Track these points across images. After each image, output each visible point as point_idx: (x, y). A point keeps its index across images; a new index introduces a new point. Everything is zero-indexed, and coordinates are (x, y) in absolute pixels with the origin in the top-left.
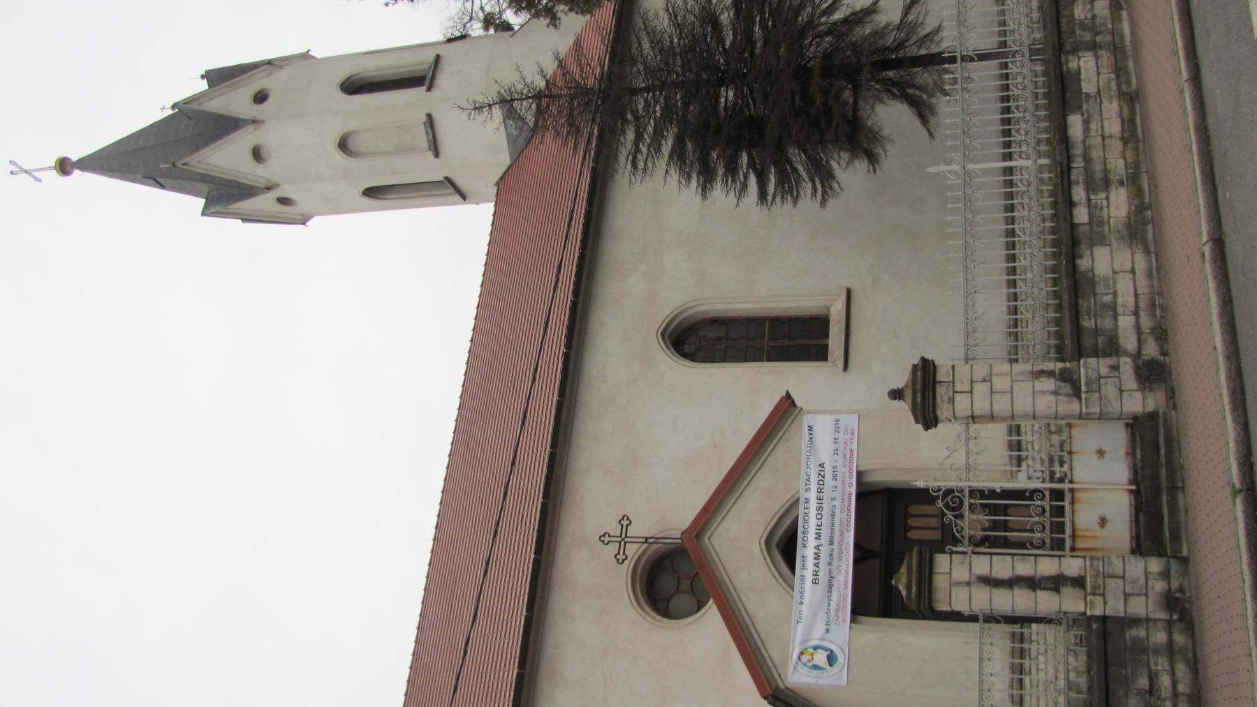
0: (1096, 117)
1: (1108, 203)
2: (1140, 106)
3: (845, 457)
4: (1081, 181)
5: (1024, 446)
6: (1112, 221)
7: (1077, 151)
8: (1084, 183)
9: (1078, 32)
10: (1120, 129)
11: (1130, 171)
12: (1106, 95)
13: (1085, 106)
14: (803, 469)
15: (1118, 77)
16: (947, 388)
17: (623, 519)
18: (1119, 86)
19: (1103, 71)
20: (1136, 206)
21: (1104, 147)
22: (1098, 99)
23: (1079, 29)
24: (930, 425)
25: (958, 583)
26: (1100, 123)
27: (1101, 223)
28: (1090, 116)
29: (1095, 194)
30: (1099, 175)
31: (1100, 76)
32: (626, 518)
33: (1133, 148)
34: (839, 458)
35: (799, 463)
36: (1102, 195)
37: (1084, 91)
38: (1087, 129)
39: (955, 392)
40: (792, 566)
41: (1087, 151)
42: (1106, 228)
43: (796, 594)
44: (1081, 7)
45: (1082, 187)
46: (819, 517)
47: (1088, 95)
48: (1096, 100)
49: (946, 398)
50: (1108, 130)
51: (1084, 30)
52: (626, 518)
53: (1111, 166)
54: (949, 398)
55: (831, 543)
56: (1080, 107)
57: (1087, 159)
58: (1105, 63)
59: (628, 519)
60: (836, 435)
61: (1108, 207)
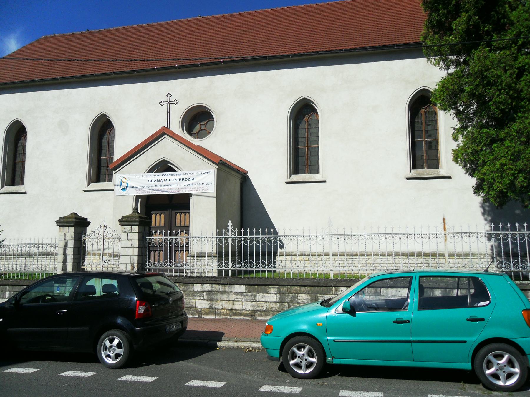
0: (244, 299)
1: (202, 300)
2: (247, 320)
3: (196, 188)
4: (213, 289)
5: (198, 258)
6: (194, 300)
7: (227, 288)
8: (212, 290)
9: (291, 295)
10: (237, 309)
11: (216, 311)
12: (255, 304)
13: (250, 294)
14: (191, 172)
15: (264, 311)
16: (129, 230)
17: (168, 95)
18: (260, 311)
19: (268, 304)
20: (200, 311)
21: (229, 301)
22: (253, 301)
23: (292, 295)
24: (59, 223)
25: (65, 236)
26: (241, 300)
27: (193, 296)
28: (244, 296)
29: (206, 294)
30: (215, 297)
31: (265, 303)
32: (169, 94)
33: (227, 314)
34: (196, 186)
35: (195, 170)
36: (206, 298)
37: (258, 294)
38: (238, 294)
39: (128, 233)
40: (151, 171)
41: (227, 293)
42: (191, 298)
43: (146, 174)
44: (306, 298)
45: (210, 289)
46: (173, 180)
47: (255, 296)
48: (253, 299)
49: (126, 230)
50: (236, 304)
51: (291, 298)
52: (169, 94)
53: (219, 302)
54: (126, 231)
55: (164, 186)
56: (249, 292)
57: (223, 292)
58: (272, 306)
59: (170, 94)
60: (205, 184)
61: (200, 299)
